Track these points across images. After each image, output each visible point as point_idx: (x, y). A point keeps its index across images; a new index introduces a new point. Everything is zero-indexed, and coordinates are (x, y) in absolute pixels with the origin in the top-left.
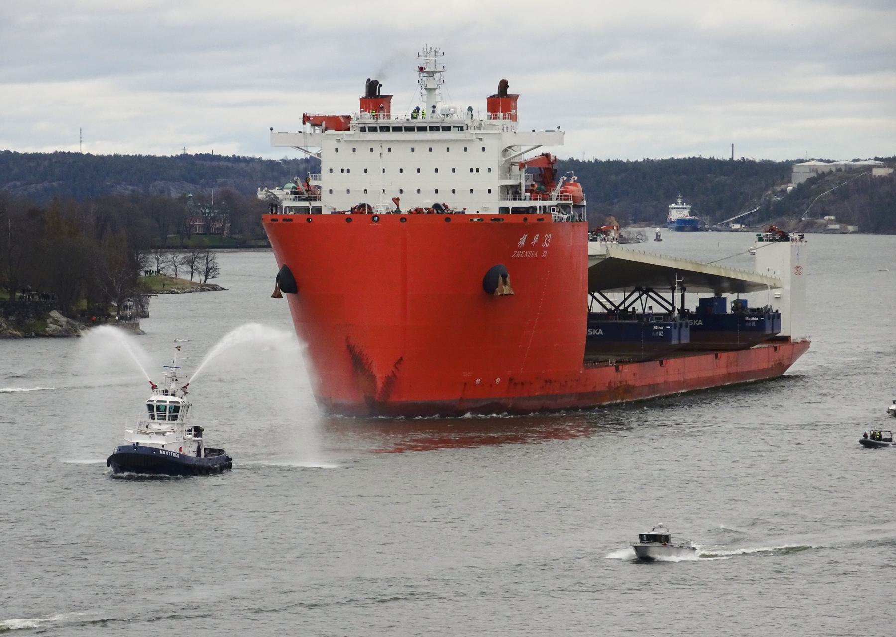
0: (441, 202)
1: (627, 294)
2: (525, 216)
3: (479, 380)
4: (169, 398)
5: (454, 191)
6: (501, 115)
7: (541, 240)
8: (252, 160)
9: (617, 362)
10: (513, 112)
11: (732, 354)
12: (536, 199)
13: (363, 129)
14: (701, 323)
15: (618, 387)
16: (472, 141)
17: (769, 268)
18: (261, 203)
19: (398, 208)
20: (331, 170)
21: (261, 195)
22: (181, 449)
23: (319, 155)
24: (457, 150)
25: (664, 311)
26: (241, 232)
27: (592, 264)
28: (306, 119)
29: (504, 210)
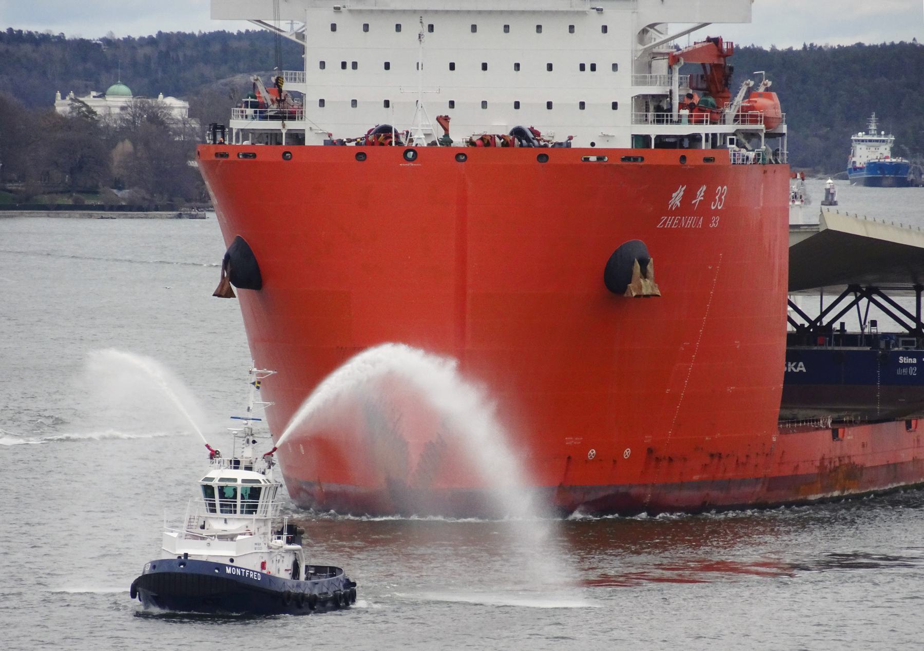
0: (526, 126)
1: (829, 300)
2: (679, 152)
3: (592, 452)
4: (241, 475)
7: (710, 196)
8: (45, 39)
9: (833, 422)
12: (700, 122)
15: (836, 468)
16: (584, 13)
18: (65, 123)
19: (447, 135)
20: (323, 65)
21: (62, 106)
22: (263, 565)
23: (301, 36)
25: (901, 329)
26: (22, 178)
27: (795, 240)
29: (641, 141)
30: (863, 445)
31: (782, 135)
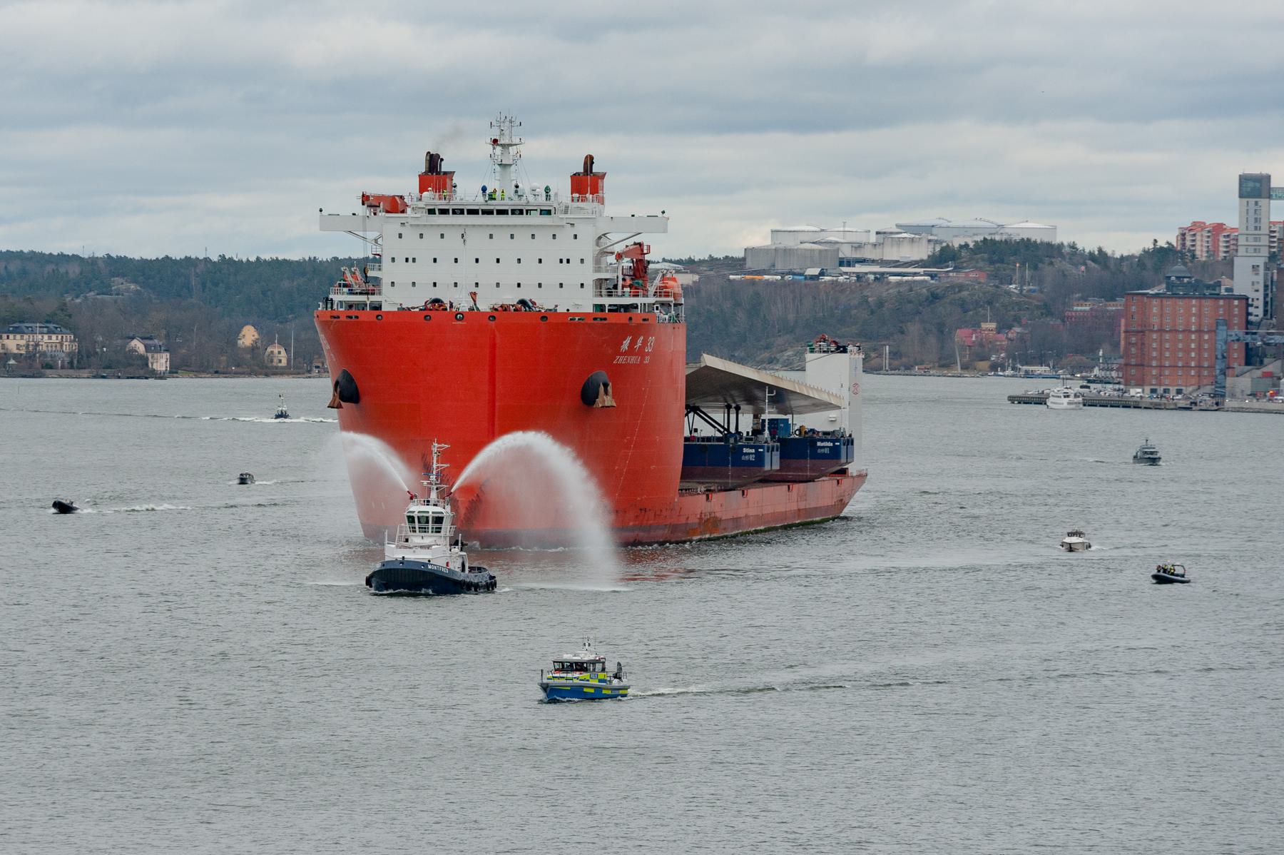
0: (527, 299)
5: (540, 285)
7: (645, 343)
8: (63, 258)
11: (802, 485)
13: (431, 212)
17: (827, 383)
20: (393, 260)
28: (365, 198)
29: (600, 308)
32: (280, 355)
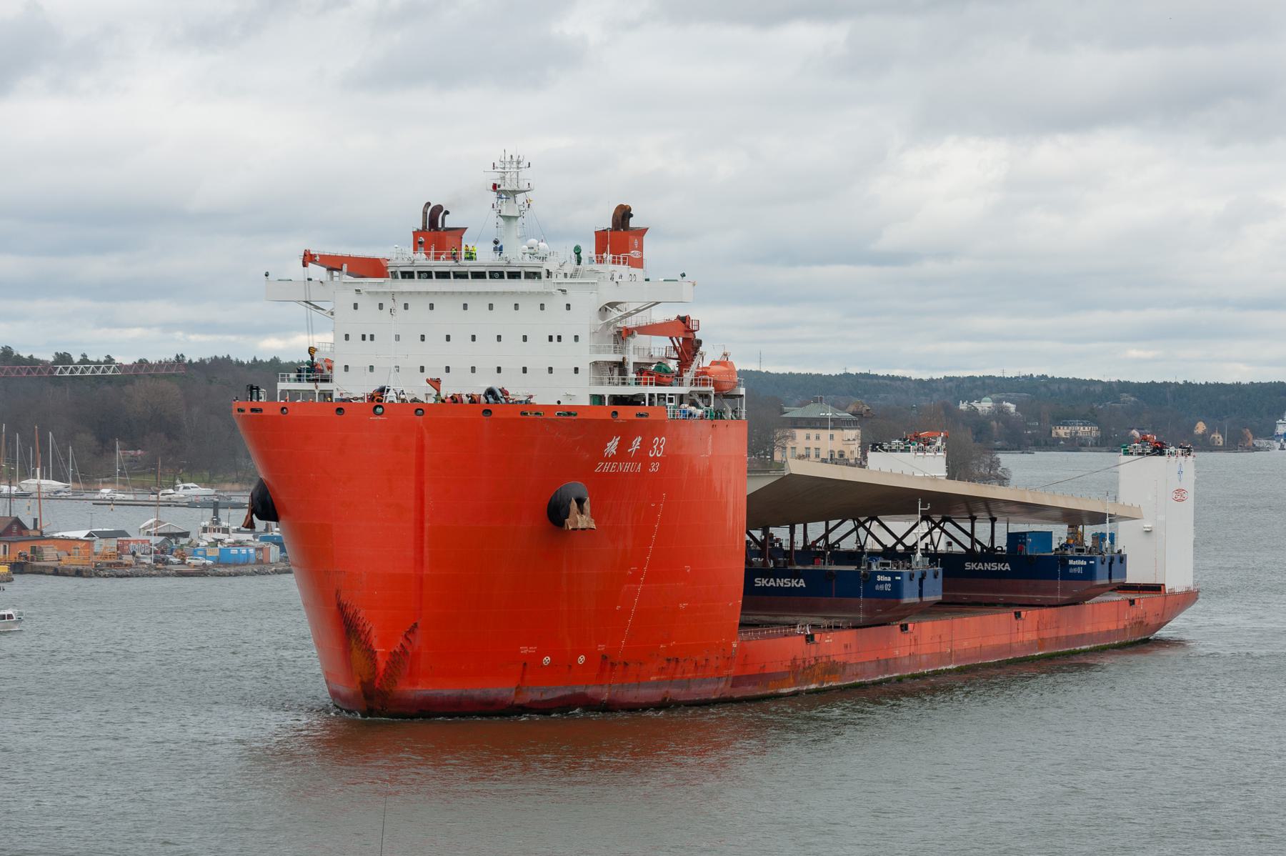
3: (547, 660)
5: (473, 369)
6: (610, 257)
7: (646, 446)
10: (634, 254)
11: (1047, 612)
14: (1007, 567)
24: (530, 307)
28: (308, 258)
30: (846, 646)
31: (741, 396)
32: (1218, 438)
